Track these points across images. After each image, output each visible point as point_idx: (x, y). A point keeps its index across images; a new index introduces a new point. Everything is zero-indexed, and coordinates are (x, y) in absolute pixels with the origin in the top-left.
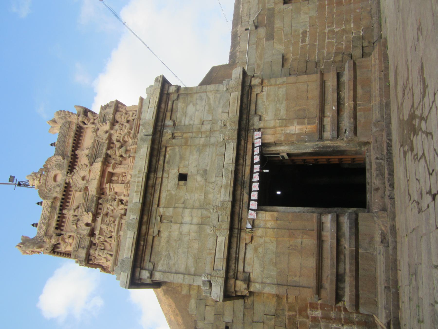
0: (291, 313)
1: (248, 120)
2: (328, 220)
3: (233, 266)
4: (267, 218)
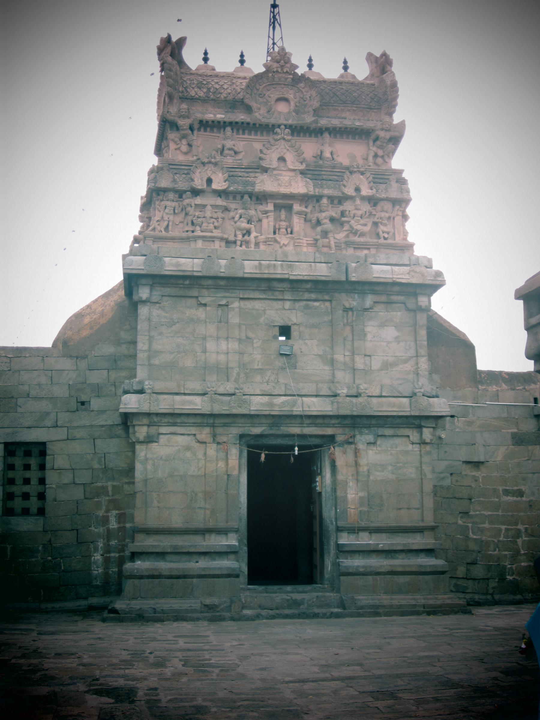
0: (110, 489)
1: (368, 427)
2: (232, 541)
3: (166, 420)
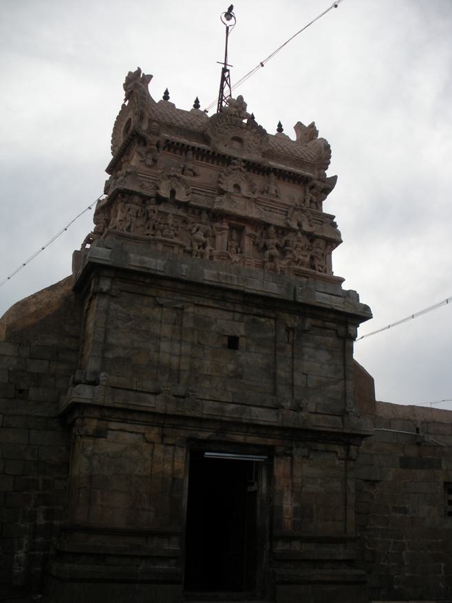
0: (41, 483)
4: (176, 464)
